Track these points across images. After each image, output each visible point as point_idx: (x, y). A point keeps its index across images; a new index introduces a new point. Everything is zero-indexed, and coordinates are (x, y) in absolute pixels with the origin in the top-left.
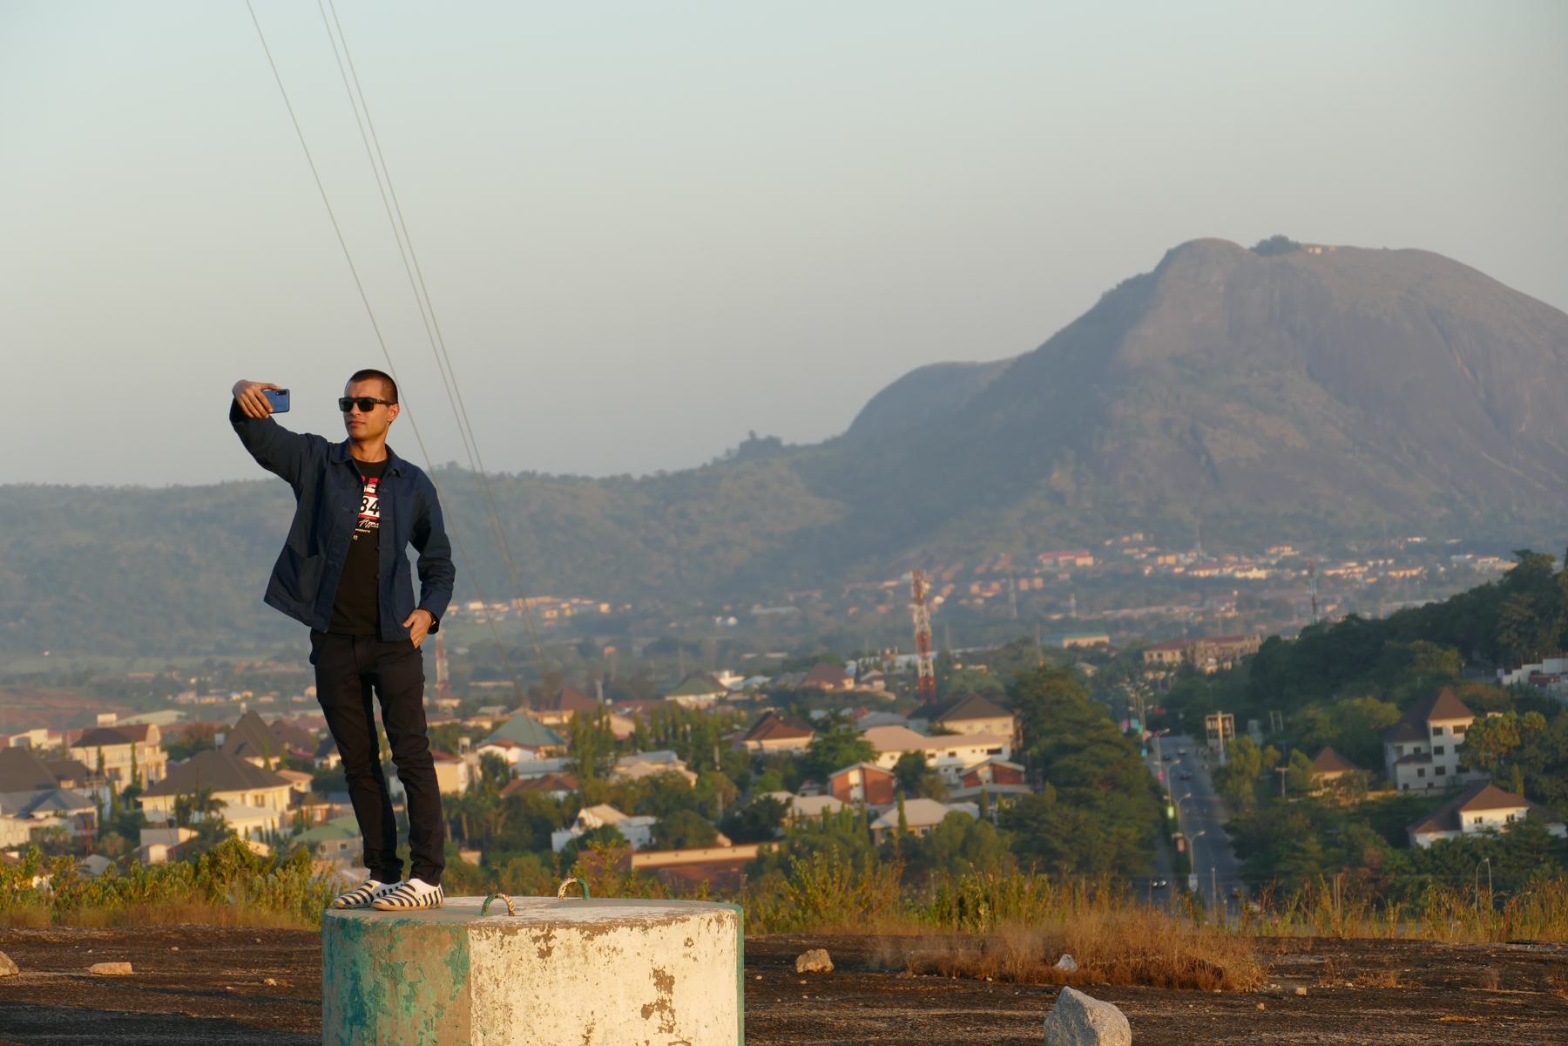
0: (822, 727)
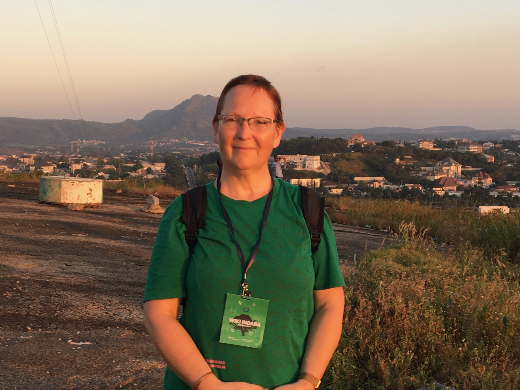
0: (135, 163)
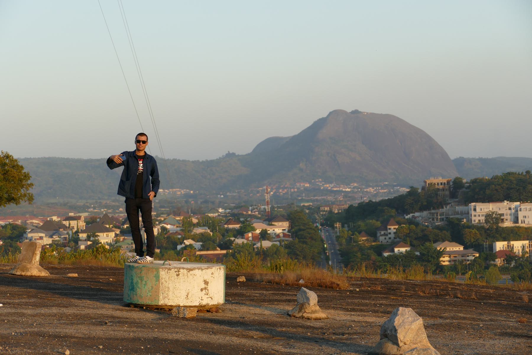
0: (243, 222)
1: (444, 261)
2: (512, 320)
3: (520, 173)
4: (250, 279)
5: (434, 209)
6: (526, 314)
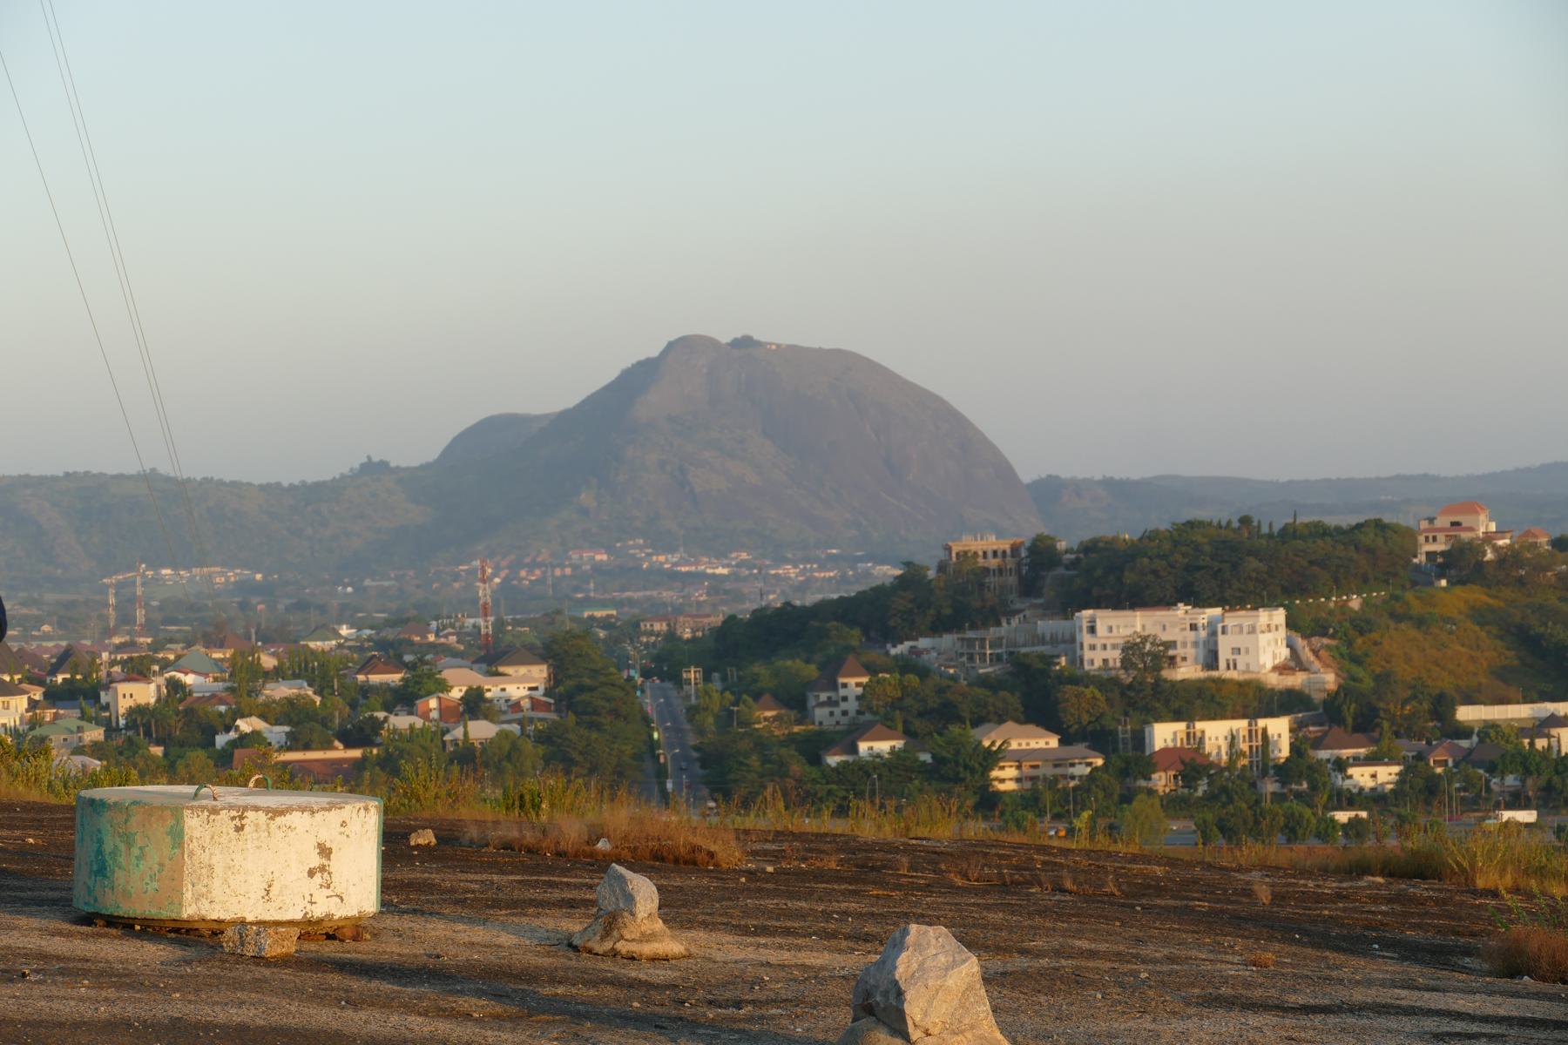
0: (411, 667)
1: (1002, 781)
2: (1229, 958)
3: (1224, 523)
4: (449, 837)
5: (973, 627)
6: (1270, 939)
